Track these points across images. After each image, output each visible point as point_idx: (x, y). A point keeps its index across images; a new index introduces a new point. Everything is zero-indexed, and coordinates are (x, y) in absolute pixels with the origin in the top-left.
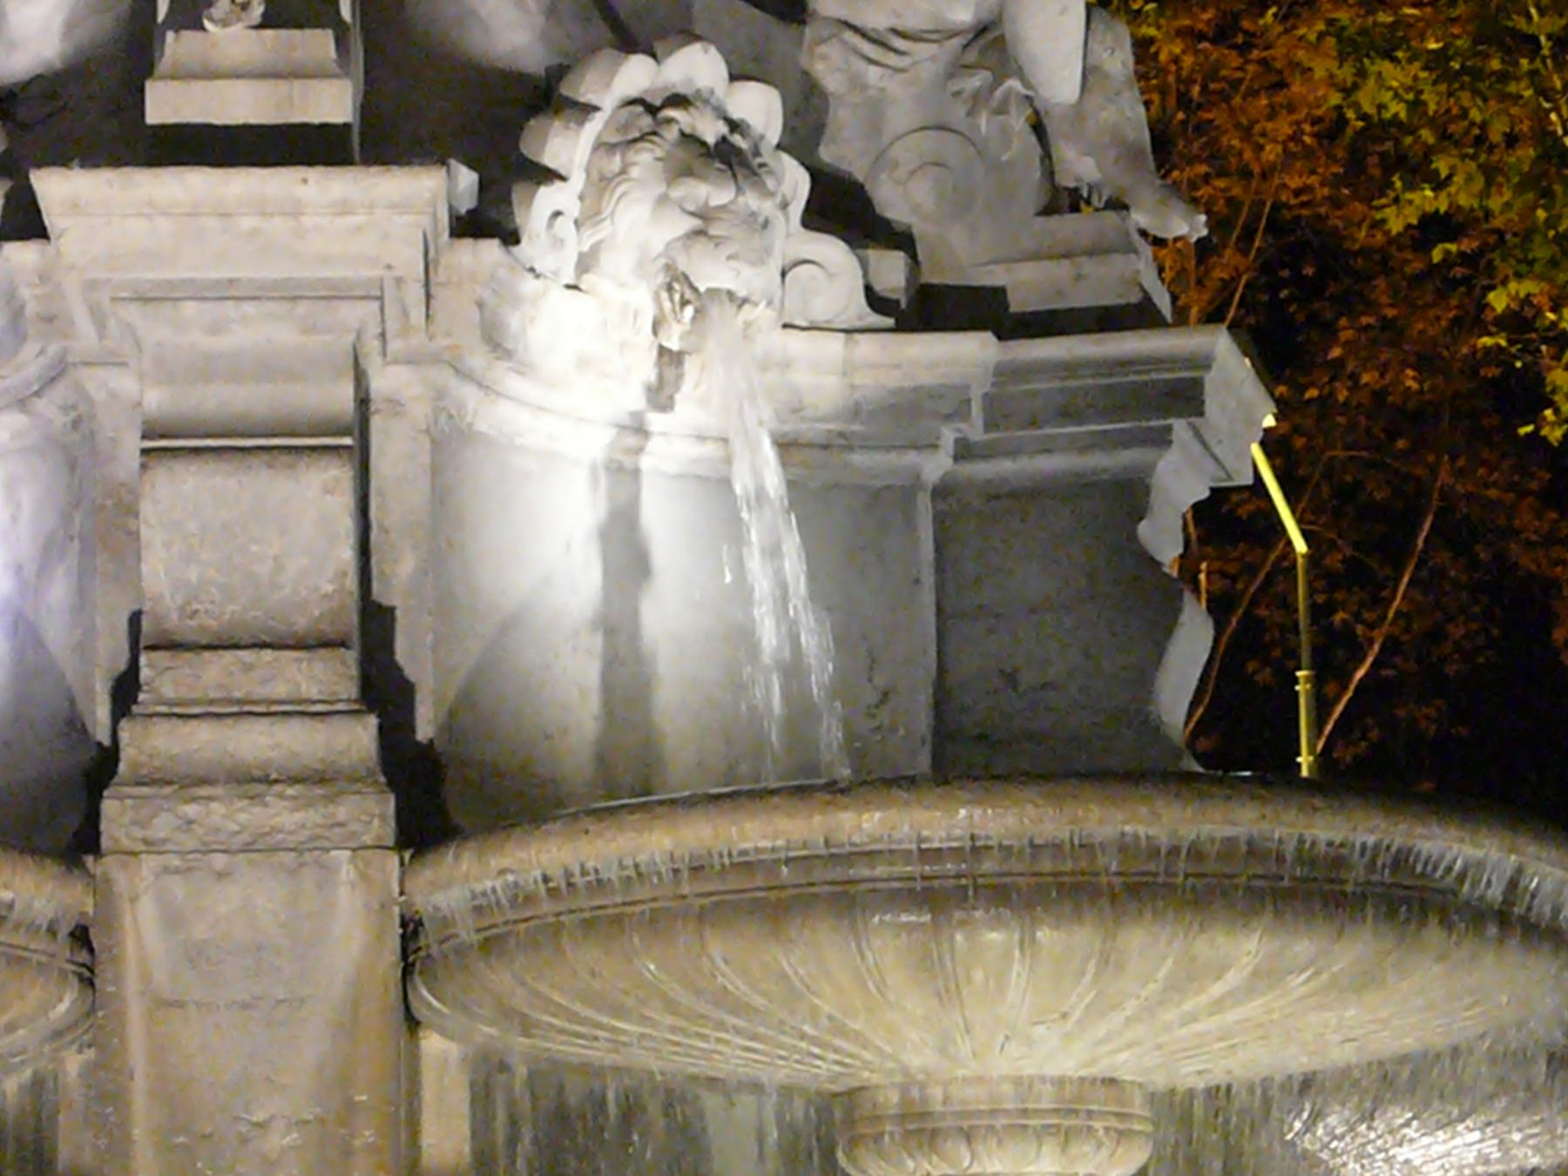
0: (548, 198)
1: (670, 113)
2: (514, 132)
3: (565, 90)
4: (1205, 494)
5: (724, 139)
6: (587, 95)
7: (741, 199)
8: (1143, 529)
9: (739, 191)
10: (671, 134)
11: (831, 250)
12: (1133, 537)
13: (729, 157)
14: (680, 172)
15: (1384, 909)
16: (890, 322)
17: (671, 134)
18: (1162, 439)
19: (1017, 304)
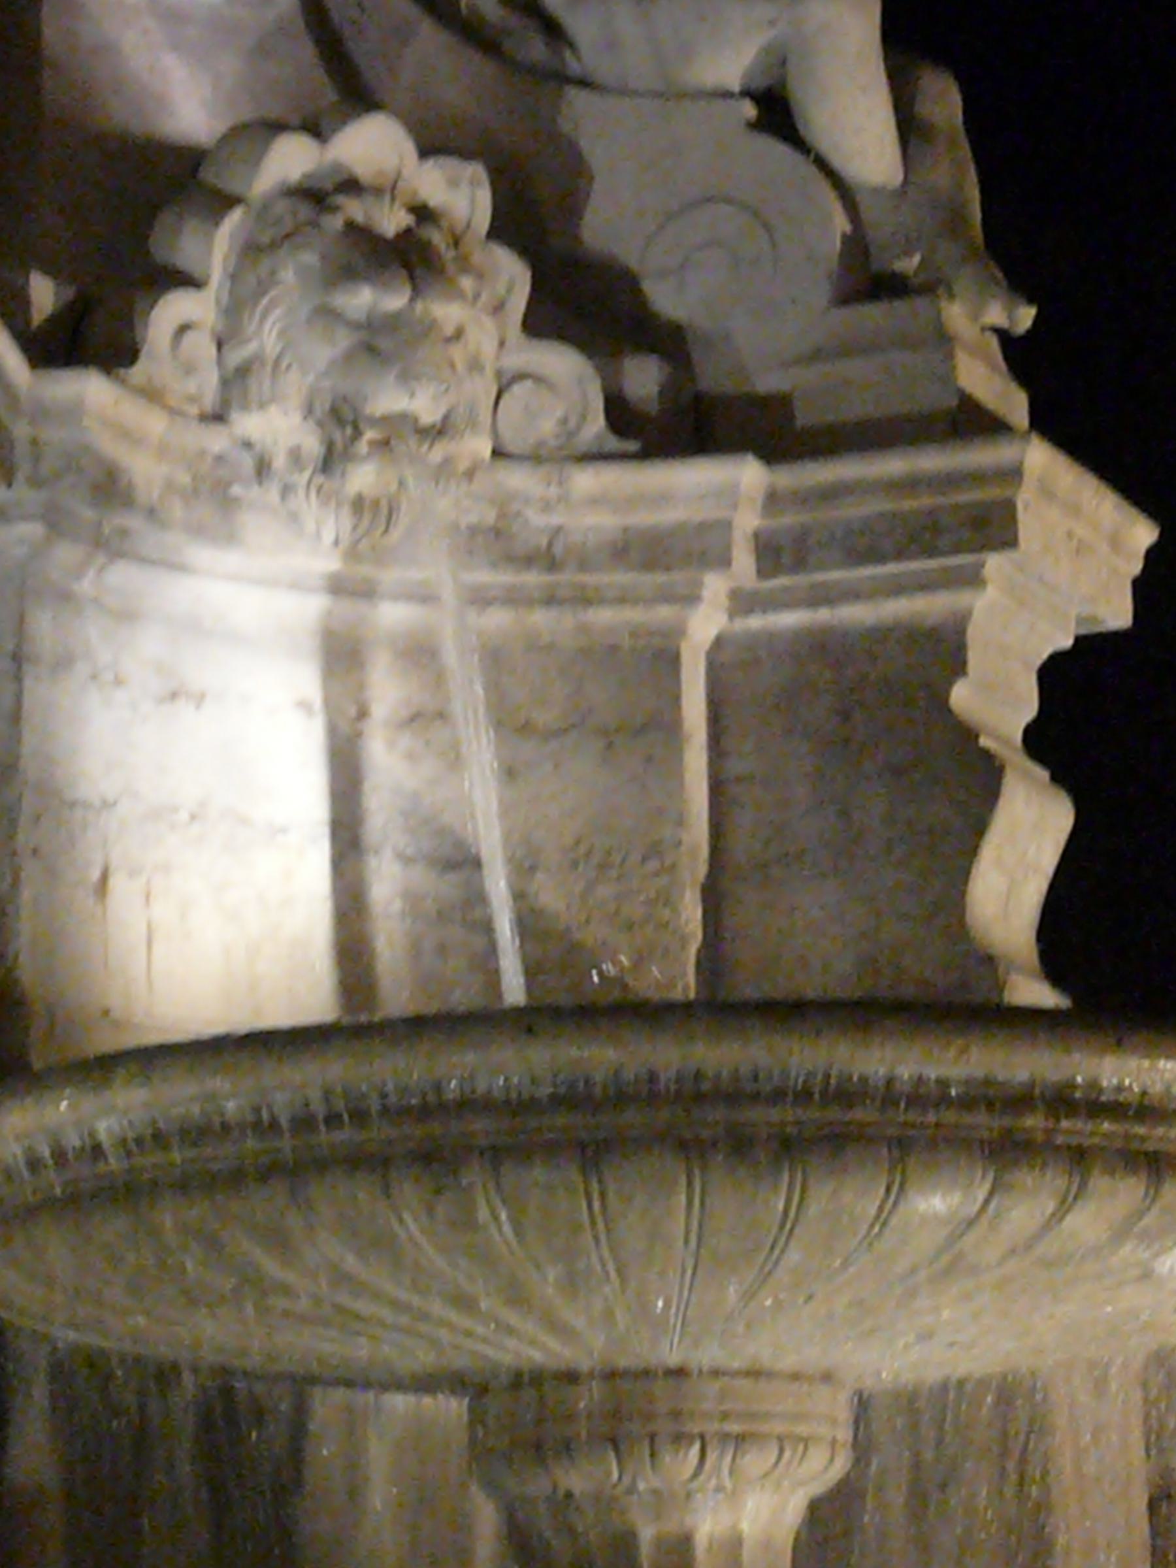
0: (173, 309)
1: (340, 199)
2: (141, 238)
3: (458, 232)
4: (1067, 643)
5: (408, 231)
6: (232, 185)
7: (419, 306)
8: (961, 696)
9: (416, 292)
10: (335, 223)
11: (562, 363)
12: (941, 703)
13: (414, 255)
14: (345, 274)
15: (1047, 1530)
16: (632, 446)
17: (335, 223)
18: (973, 579)
19: (804, 417)
